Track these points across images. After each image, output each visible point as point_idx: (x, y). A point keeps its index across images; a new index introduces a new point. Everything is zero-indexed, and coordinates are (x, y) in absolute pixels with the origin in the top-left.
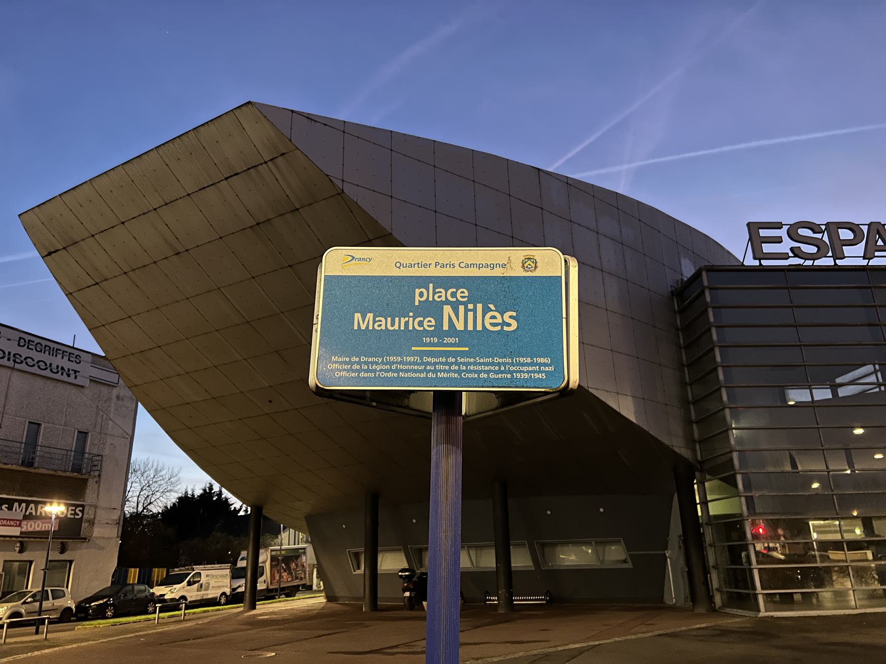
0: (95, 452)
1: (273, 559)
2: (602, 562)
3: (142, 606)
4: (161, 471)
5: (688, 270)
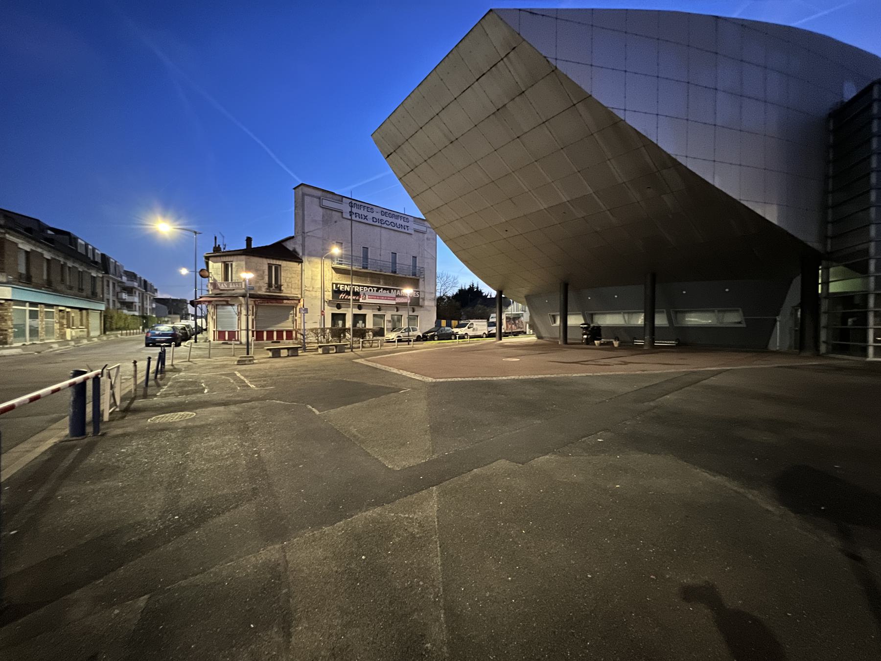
0: (421, 266)
1: (507, 318)
2: (722, 323)
3: (449, 336)
4: (449, 277)
5: (850, 92)
